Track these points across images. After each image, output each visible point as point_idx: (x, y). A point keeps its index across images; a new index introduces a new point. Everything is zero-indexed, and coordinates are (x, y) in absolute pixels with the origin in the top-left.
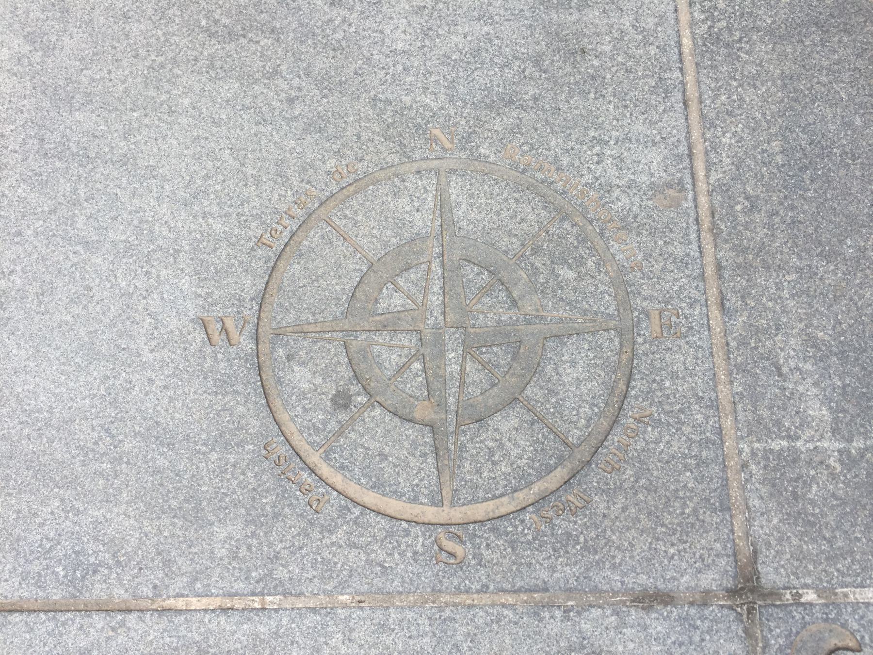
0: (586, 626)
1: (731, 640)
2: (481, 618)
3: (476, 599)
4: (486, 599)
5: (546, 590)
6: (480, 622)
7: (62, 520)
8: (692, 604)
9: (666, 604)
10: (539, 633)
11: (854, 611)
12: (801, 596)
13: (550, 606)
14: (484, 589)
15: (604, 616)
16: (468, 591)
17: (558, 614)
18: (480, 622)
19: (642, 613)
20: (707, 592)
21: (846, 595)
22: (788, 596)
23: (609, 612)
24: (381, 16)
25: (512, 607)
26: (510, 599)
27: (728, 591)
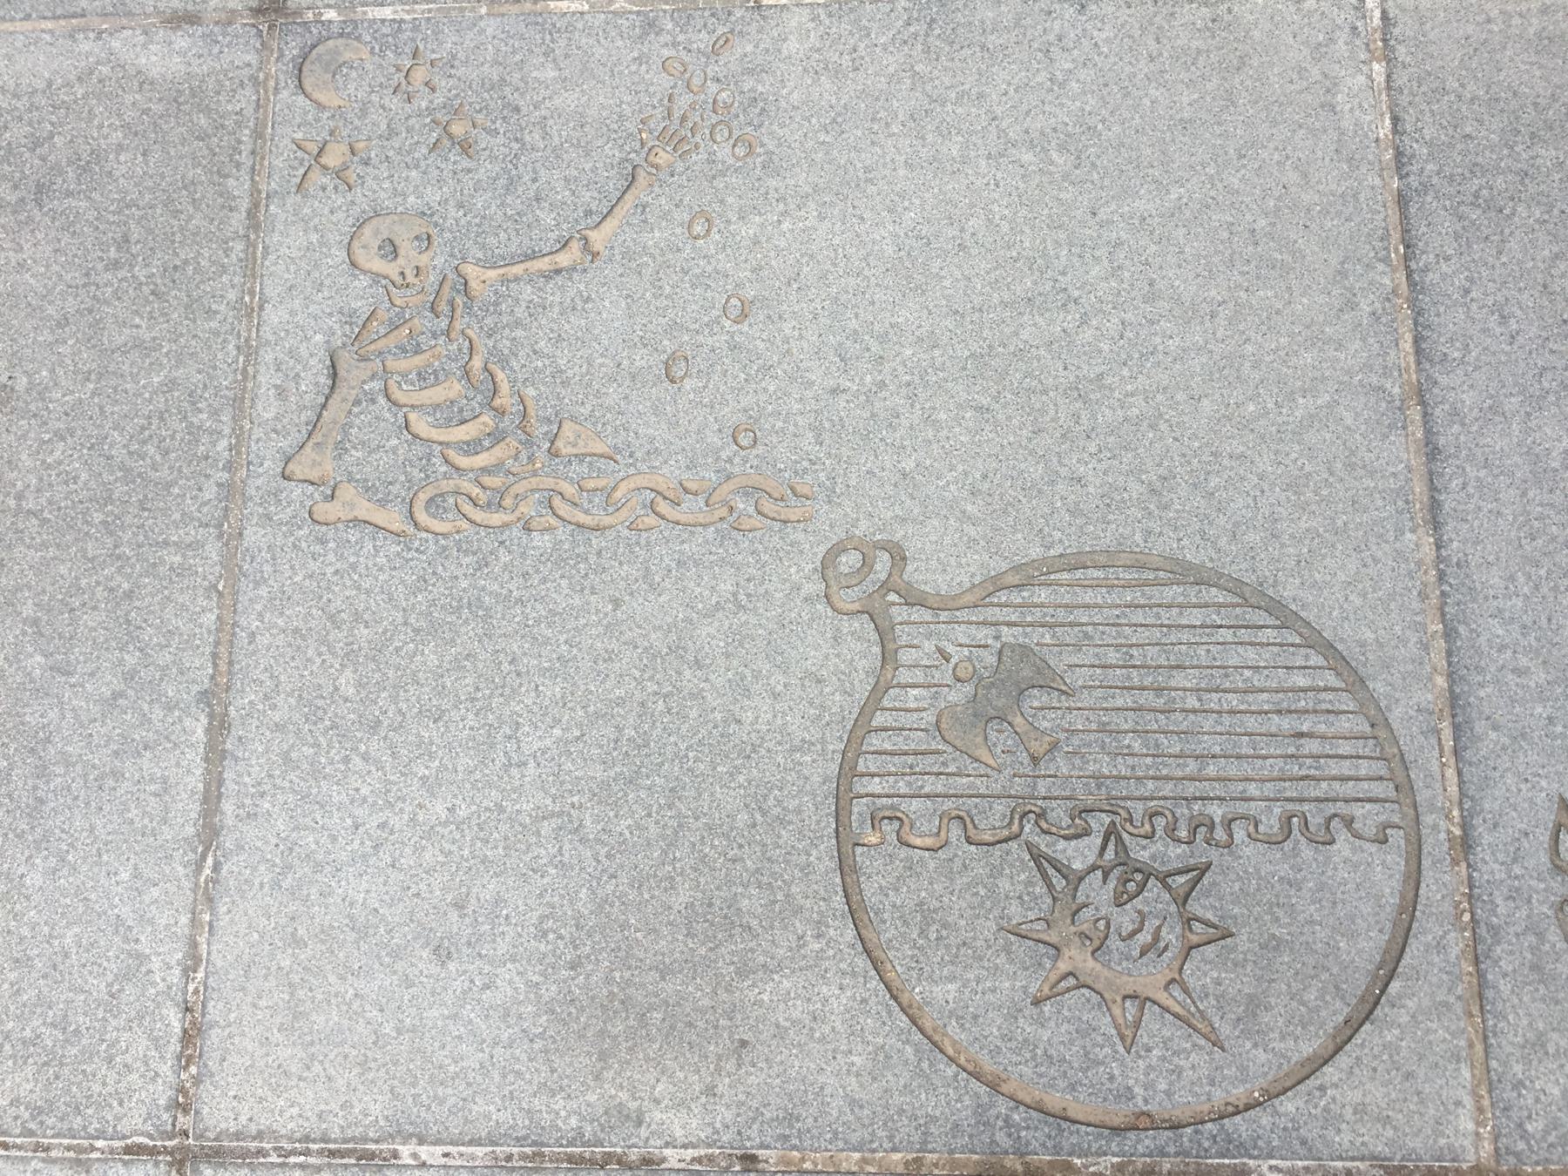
0: (116, 44)
1: (248, 52)
2: (20, 41)
3: (19, 26)
4: (28, 25)
5: (83, 16)
6: (18, 44)
7: (1085, 416)
8: (217, 23)
9: (192, 23)
10: (72, 52)
11: (370, 27)
12: (321, 14)
13: (84, 30)
14: (27, 17)
15: (134, 35)
16: (12, 20)
17: (92, 35)
18: (18, 44)
19: (170, 32)
20: (233, 11)
21: (365, 13)
22: (310, 15)
23: (138, 32)
24: (935, 446)
25: (51, 32)
26: (49, 25)
27: (251, 9)
